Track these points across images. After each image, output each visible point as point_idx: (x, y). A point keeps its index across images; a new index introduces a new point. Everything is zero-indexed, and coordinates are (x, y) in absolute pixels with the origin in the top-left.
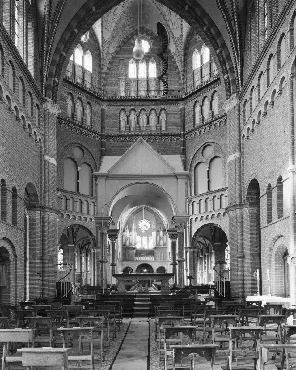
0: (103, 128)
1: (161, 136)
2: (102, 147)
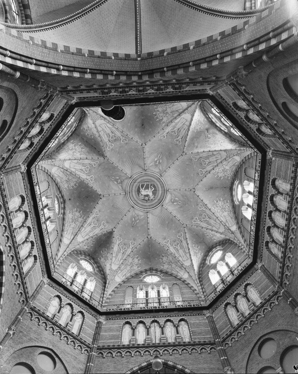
0: (95, 339)
1: (193, 345)
2: (227, 360)
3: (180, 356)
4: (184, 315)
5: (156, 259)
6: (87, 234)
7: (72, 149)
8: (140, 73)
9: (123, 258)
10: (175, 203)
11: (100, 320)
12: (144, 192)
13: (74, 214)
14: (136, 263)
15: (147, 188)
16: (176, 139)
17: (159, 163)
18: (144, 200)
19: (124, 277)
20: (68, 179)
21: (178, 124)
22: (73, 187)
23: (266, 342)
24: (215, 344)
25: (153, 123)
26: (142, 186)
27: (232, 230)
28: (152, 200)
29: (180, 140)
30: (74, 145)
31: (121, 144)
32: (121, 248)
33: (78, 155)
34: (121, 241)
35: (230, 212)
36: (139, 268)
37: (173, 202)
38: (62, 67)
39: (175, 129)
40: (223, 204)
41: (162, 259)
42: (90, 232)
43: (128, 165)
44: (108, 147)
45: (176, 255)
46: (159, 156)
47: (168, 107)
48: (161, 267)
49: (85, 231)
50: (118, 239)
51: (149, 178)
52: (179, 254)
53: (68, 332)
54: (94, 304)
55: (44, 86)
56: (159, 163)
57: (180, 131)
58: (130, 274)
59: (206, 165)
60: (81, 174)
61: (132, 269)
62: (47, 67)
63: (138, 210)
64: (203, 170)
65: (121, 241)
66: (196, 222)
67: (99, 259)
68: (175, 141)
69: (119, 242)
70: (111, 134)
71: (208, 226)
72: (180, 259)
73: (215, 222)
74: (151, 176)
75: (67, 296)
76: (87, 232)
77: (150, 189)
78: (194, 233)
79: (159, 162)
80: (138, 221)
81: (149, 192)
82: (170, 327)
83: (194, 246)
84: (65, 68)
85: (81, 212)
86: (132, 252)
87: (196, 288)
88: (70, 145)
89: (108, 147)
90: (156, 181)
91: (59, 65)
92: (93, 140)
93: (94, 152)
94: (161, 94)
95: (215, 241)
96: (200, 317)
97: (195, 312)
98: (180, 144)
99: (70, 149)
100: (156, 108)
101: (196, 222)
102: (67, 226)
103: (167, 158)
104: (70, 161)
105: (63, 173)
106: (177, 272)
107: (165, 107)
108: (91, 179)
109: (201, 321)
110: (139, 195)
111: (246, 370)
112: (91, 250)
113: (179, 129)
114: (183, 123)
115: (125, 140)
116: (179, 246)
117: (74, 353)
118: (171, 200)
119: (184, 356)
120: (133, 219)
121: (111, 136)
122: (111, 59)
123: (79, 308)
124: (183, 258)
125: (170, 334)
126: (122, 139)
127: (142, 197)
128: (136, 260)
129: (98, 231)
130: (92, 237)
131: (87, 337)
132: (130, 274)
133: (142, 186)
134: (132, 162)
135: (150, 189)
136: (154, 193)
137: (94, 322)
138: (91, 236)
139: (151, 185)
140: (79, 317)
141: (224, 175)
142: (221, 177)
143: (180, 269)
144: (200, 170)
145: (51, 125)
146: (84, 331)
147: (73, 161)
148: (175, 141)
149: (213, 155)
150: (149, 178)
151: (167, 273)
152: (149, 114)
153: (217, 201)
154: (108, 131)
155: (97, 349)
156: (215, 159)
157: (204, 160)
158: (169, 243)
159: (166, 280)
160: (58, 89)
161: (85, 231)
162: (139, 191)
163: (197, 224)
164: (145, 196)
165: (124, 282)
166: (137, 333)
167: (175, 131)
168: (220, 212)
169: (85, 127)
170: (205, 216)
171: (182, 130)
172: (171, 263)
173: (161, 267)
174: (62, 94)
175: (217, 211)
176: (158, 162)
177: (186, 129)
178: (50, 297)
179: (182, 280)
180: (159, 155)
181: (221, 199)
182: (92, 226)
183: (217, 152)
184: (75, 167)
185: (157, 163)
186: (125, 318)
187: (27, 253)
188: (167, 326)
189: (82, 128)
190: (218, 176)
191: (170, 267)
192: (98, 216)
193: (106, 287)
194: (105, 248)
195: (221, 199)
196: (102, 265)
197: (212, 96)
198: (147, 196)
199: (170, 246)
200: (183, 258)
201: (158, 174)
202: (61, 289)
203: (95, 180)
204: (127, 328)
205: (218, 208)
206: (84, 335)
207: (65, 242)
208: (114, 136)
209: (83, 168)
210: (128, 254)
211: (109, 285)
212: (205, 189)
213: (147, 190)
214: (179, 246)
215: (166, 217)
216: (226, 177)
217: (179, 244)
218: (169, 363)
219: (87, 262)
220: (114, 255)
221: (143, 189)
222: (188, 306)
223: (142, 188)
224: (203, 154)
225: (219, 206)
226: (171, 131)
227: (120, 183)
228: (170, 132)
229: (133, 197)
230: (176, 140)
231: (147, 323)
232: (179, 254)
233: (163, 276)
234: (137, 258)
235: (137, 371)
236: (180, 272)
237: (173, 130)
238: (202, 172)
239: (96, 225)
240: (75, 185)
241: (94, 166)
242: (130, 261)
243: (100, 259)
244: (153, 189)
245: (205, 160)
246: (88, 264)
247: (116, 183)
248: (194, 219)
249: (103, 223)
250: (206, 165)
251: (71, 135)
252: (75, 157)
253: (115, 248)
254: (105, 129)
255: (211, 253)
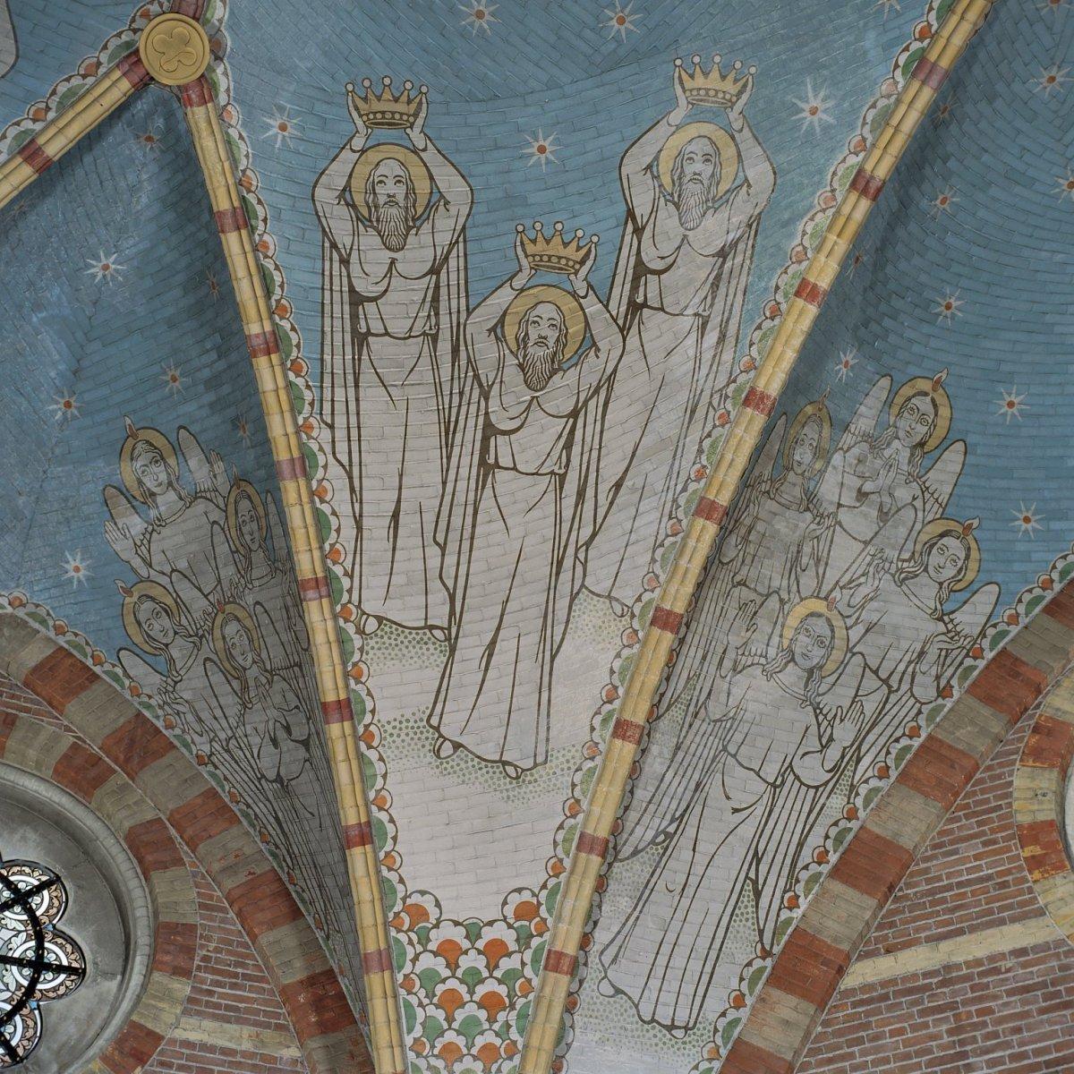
16: (445, 226)
21: (539, 566)
57: (448, 431)
68: (450, 183)
98: (337, 175)
100: (956, 591)
111: (502, 755)
113: (487, 468)
114: (471, 647)
148: (450, 183)
167: (536, 380)
177: (377, 527)
193: (335, 647)
226: (592, 369)
228: (607, 337)
230: (438, 200)
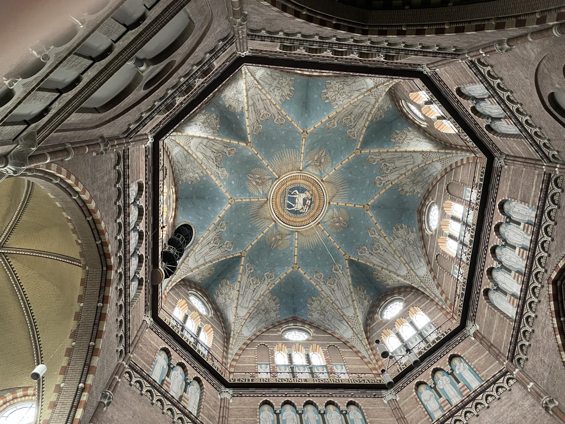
3: (555, 242)
4: (493, 200)
5: (405, 200)
6: (346, 298)
7: (225, 299)
8: (105, 269)
9: (393, 253)
10: (323, 161)
11: (472, 331)
12: (299, 206)
13: (315, 310)
14: (406, 234)
15: (293, 200)
17: (260, 180)
18: (310, 207)
19: (422, 259)
20: (263, 311)
22: (276, 304)
23: (556, 100)
24: (550, 174)
25: (202, 185)
26: (290, 206)
27: (372, 86)
28: (312, 195)
29: (229, 149)
30: (220, 295)
31: (227, 231)
32: (376, 252)
33: (234, 294)
34: (366, 249)
35: (346, 83)
36: (414, 230)
37: (321, 163)
38: (81, 385)
39: (212, 156)
40: (332, 90)
41: (406, 192)
42: (343, 293)
43: (258, 223)
44: (229, 250)
45: (402, 172)
46: (320, 153)
47: (180, 168)
48: (419, 196)
49: (341, 302)
50: (362, 253)
51: (279, 195)
52: (401, 168)
53: (470, 398)
54: (445, 332)
55: (107, 395)
56: (259, 179)
58: (419, 249)
59: (268, 113)
60: (260, 291)
61: (412, 242)
62: (77, 408)
63: (324, 217)
64: (277, 118)
65: (366, 249)
66: (355, 133)
67: (389, 287)
69: (367, 252)
70: (211, 245)
71: (363, 117)
72: (409, 167)
73: (358, 107)
74: (277, 193)
75: (421, 371)
76: (343, 298)
77: (295, 196)
78: (374, 136)
79: (258, 178)
80: (341, 218)
81: (300, 198)
82: (508, 231)
83: (393, 140)
84: (83, 379)
85: (314, 299)
86: (385, 237)
87: (459, 159)
88: (220, 300)
89: (229, 250)
90: (284, 187)
91: (78, 389)
92: (218, 268)
93: (234, 268)
94: (148, 208)
95: (391, 106)
96: (504, 175)
97: (493, 181)
99: (224, 301)
101: (355, 133)
102: (329, 325)
103: (254, 168)
104: (239, 307)
105: (253, 318)
106: (430, 175)
107: (180, 171)
108: (269, 277)
109: (510, 177)
110: (302, 213)
112: (372, 294)
114: (204, 147)
115: (221, 225)
116: (389, 165)
117: (505, 404)
118: (316, 166)
119: (557, 235)
120: (337, 224)
121: (214, 245)
122: (82, 307)
123: (443, 358)
124: (409, 163)
125: (518, 236)
126: (220, 230)
127: (306, 208)
128: (401, 232)
129: (346, 280)
130: (351, 293)
131: (489, 369)
132: (419, 249)
133: (290, 206)
134: (255, 217)
135: (295, 196)
136: (302, 191)
137: (472, 343)
138: (349, 294)
139: (290, 193)
140: (458, 364)
141: (287, 87)
142: (290, 90)
143: (426, 171)
144: (276, 121)
145: (176, 351)
146: (479, 369)
147: (239, 303)
149: (254, 104)
150: (279, 195)
151: (430, 192)
152: (191, 189)
153: (327, 98)
154: (206, 249)
155: (512, 361)
156: (261, 102)
157: (261, 116)
158: (382, 179)
159: (439, 199)
160: (120, 361)
161: (341, 302)
162: (296, 212)
163: (358, 133)
164: (304, 204)
165: (429, 263)
166: (504, 286)
168: (344, 96)
169: (198, 278)
170: (347, 119)
171: (215, 147)
172: (416, 181)
173: (419, 196)
174: (129, 352)
175: (341, 102)
176: (258, 180)
177: (214, 143)
178: (414, 400)
179: (343, 340)
180: (249, 178)
181: (325, 91)
182: (336, 288)
183: (250, 99)
184: (249, 301)
185: (260, 182)
186: (477, 293)
187: (340, 418)
188: (506, 234)
189: (200, 282)
190: (288, 95)
191: (421, 183)
192: (323, 276)
194: (373, 273)
195: (325, 91)
196: (397, 285)
197: (154, 137)
198: (305, 200)
199: (386, 179)
200: (409, 163)
201: (275, 183)
202: (408, 375)
203: (271, 272)
204: (494, 297)
205: (337, 98)
206: (486, 371)
207: (350, 337)
208: (214, 240)
209: (252, 287)
210: (387, 243)
211: (427, 289)
212: (306, 116)
213: (297, 201)
214: (389, 165)
215: (342, 176)
216: (291, 83)
217: (386, 164)
218: (553, 277)
219: (389, 307)
220: (385, 267)
221: (294, 205)
222: (480, 189)
223: (293, 207)
224: (251, 119)
225: (334, 98)
226: (215, 161)
227: (282, 237)
229: (304, 221)
231: (493, 264)
232: (401, 168)
233: (433, 199)
234: (398, 229)
235: (559, 321)
236: (430, 173)
237: (214, 159)
238: (279, 120)
239: (336, 282)
240: (274, 300)
241: (252, 271)
242: (400, 243)
243: (388, 285)
244: (296, 191)
245: (262, 114)
246: (391, 305)
247: (280, 242)
248: (351, 136)
249: (334, 270)
250: (268, 113)
251: (207, 297)
252: (234, 298)
253: (375, 260)
254: (202, 254)
255: (409, 116)
